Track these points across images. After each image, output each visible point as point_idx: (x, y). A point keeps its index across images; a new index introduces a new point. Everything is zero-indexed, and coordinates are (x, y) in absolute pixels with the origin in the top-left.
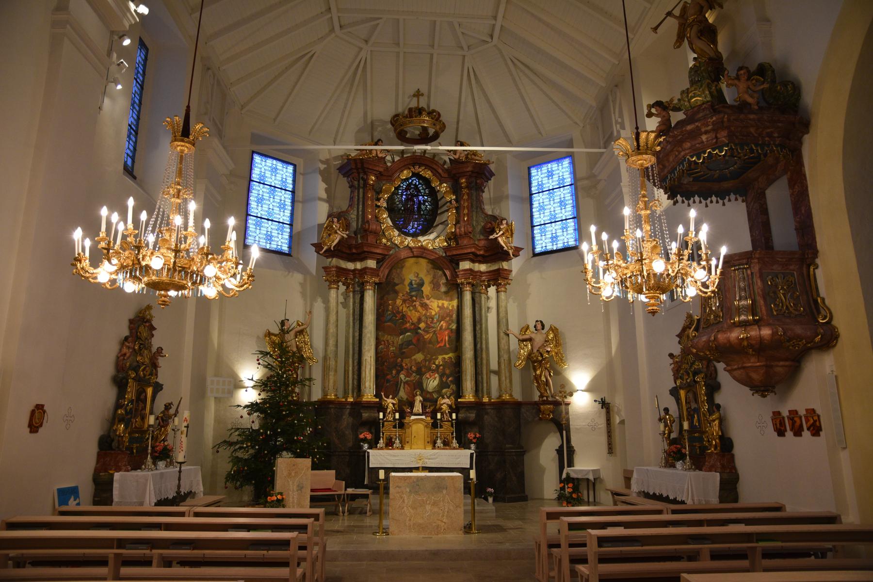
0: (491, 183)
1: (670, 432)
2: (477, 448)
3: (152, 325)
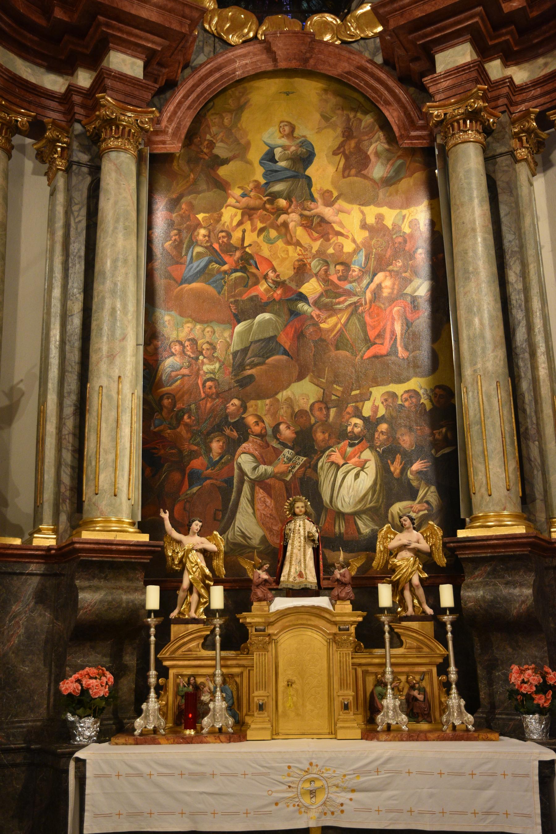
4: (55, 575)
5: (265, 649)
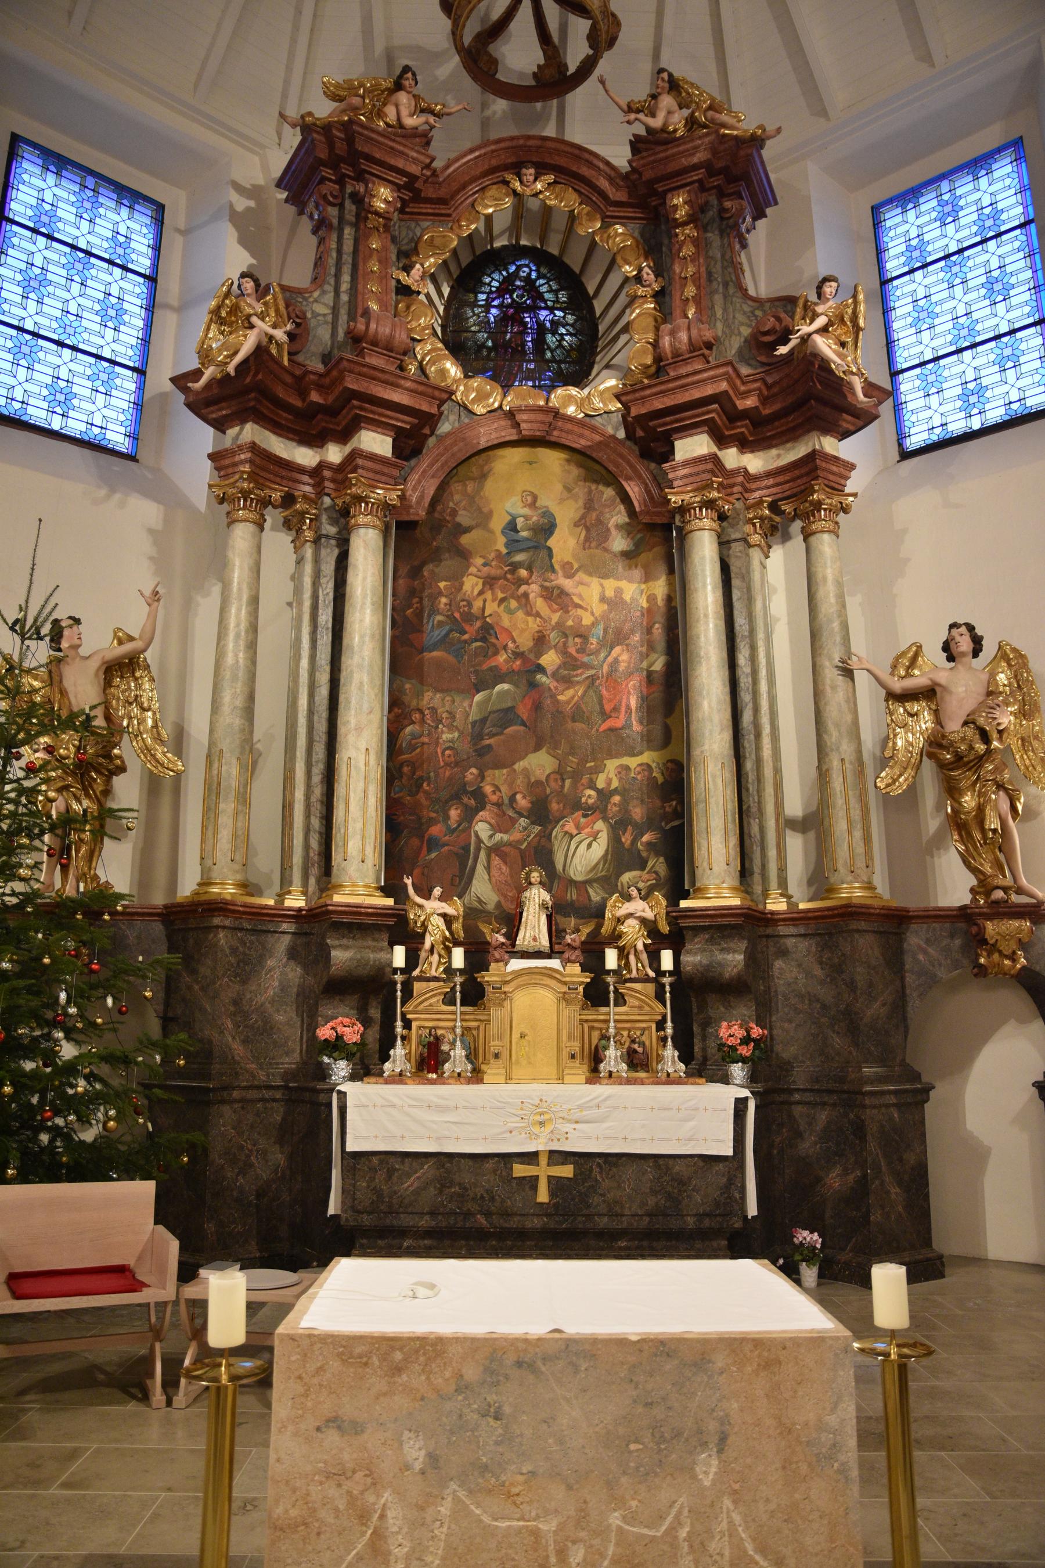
2: (753, 1079)
4: (306, 934)
5: (501, 1005)
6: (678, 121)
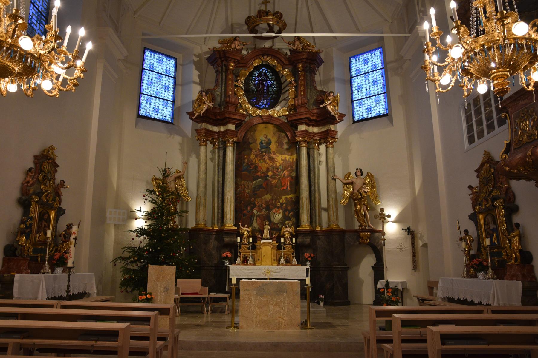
0: (321, 68)
1: (470, 249)
2: (311, 265)
3: (55, 163)
6: (300, 48)
